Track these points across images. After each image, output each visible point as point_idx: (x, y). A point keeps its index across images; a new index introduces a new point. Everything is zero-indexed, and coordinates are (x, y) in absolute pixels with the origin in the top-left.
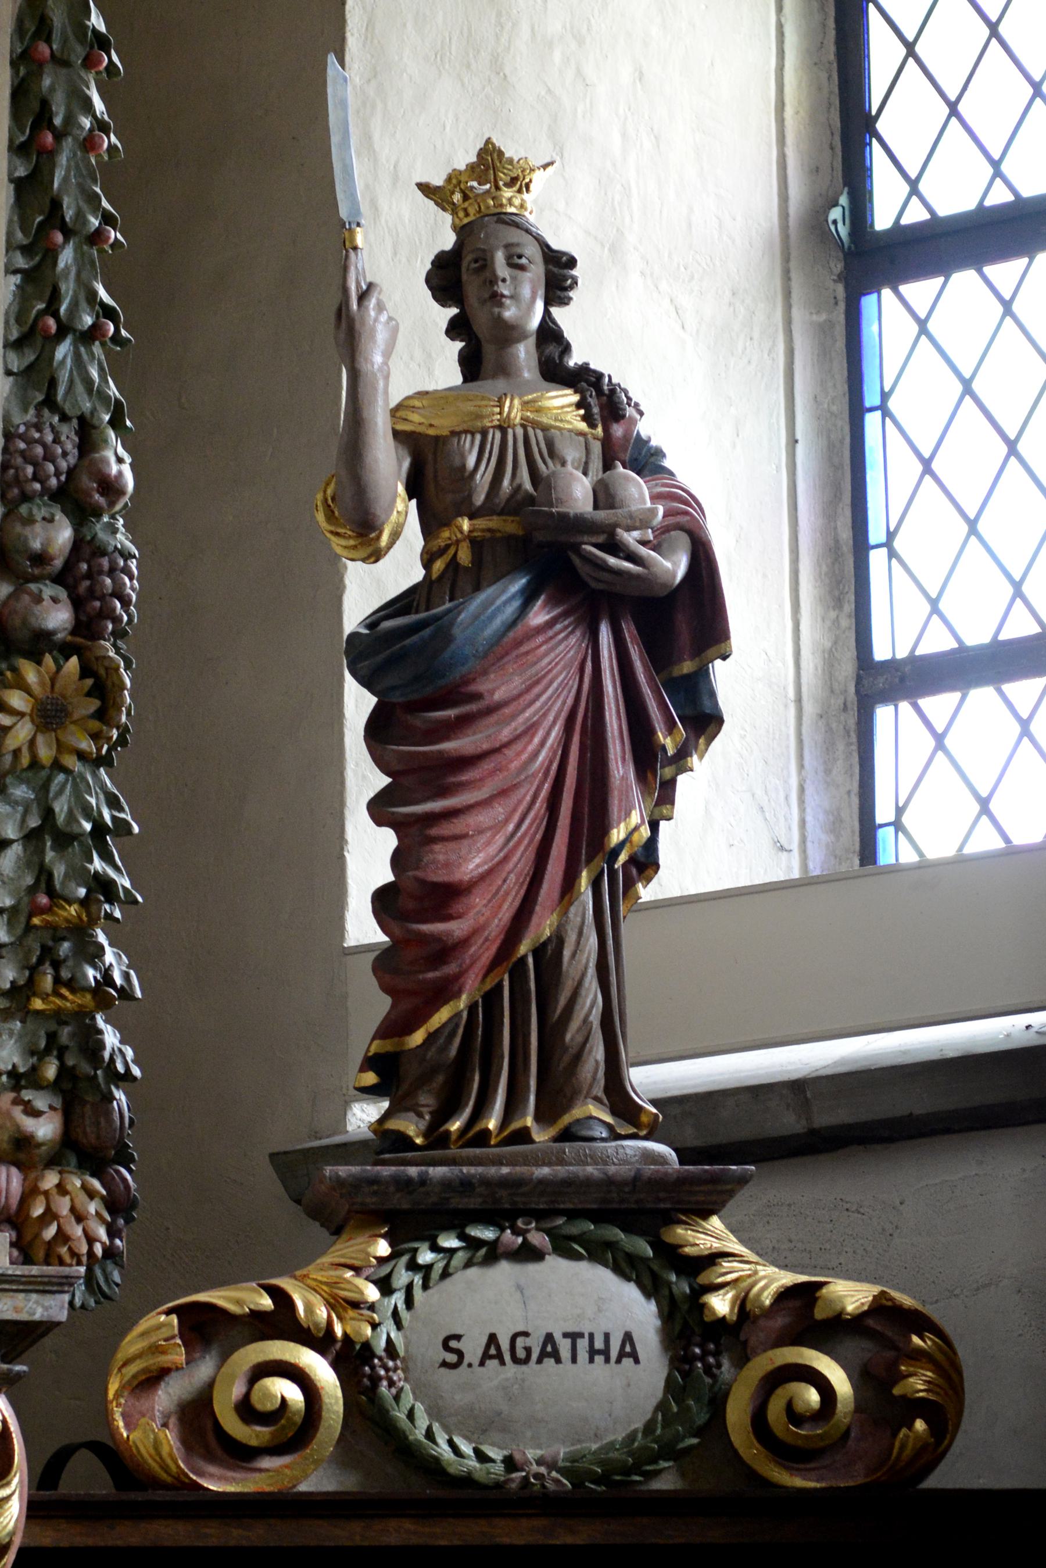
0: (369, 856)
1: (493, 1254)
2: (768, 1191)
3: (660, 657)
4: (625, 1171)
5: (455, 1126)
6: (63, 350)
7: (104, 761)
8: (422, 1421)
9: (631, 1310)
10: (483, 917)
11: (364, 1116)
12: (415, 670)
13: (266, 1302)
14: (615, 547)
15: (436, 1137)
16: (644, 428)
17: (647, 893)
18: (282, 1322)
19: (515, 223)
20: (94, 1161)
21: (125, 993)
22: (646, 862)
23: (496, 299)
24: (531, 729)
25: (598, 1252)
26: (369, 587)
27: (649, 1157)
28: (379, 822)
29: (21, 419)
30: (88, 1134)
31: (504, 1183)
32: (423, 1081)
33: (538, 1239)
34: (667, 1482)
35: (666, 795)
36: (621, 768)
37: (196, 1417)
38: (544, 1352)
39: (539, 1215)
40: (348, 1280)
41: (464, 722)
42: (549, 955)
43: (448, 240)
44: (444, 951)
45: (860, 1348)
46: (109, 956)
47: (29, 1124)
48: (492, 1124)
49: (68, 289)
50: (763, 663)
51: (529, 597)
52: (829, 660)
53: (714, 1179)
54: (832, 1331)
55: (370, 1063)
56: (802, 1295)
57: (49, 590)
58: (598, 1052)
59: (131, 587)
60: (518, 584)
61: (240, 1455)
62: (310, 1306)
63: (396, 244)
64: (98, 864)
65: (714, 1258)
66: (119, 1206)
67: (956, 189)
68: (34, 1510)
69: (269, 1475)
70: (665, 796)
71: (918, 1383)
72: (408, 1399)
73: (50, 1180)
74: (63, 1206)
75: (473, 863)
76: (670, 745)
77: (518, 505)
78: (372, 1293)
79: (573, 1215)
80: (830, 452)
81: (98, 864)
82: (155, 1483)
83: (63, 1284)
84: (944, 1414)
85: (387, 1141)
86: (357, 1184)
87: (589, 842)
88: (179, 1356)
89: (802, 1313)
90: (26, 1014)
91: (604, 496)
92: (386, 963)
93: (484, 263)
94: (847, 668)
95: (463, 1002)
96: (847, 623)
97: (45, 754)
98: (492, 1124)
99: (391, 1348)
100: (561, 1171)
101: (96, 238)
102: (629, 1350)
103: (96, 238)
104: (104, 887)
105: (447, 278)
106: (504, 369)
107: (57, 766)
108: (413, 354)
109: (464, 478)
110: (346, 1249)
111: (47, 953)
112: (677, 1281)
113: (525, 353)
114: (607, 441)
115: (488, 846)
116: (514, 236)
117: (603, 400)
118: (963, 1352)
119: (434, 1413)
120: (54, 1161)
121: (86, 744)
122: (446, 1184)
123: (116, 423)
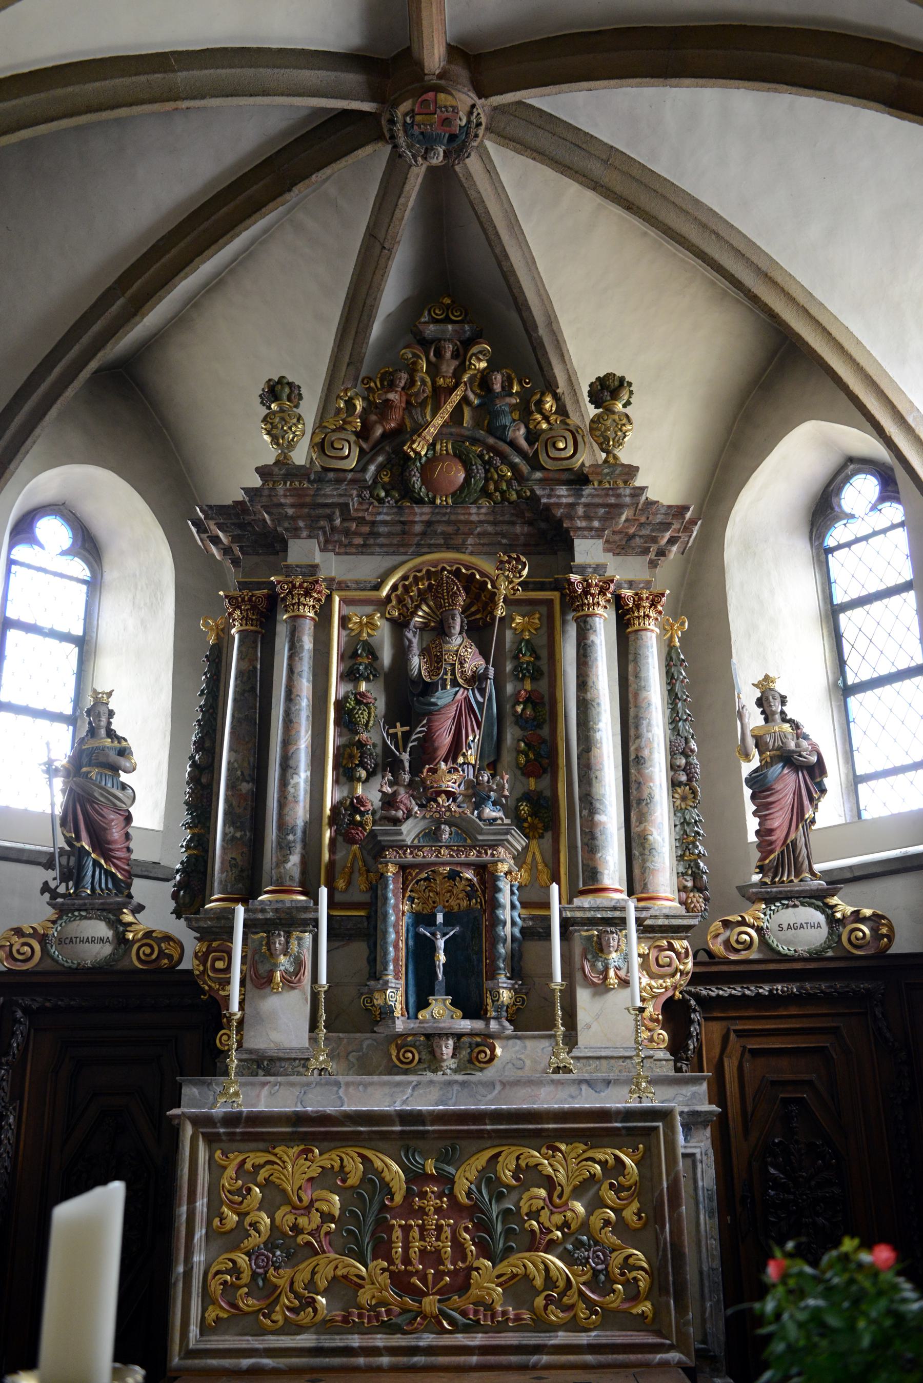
0: (753, 824)
1: (788, 906)
2: (846, 889)
3: (812, 777)
4: (815, 888)
5: (777, 880)
6: (680, 724)
7: (695, 807)
8: (775, 943)
9: (819, 917)
10: (779, 836)
11: (756, 878)
12: (760, 785)
13: (740, 919)
14: (801, 756)
15: (773, 883)
16: (804, 730)
17: (813, 828)
18: (743, 923)
19: (773, 690)
20: (700, 890)
21: (704, 855)
22: (813, 821)
23: (770, 706)
24: (786, 795)
25: (810, 905)
26: (747, 769)
27: (820, 884)
28: (755, 816)
29: (673, 738)
30: (699, 885)
31: (788, 891)
32: (769, 870)
33: (797, 903)
34: (830, 954)
35: (816, 807)
36: (806, 802)
37: (727, 943)
38: (800, 929)
39: (797, 898)
40: (756, 913)
41: (772, 794)
42: (794, 843)
43: (759, 695)
44: (771, 843)
45: (870, 923)
46: (700, 847)
47: (686, 883)
48: (785, 879)
49: (680, 711)
50: (834, 779)
51: (783, 767)
52: (847, 776)
53: (835, 888)
54: (864, 920)
55: (758, 867)
56: (857, 912)
57: (681, 773)
58: (806, 862)
59: (698, 771)
60: (781, 764)
61: (737, 951)
62: (749, 919)
63: (747, 696)
64: (696, 829)
65: (836, 905)
66: (706, 899)
67: (866, 675)
68: (695, 964)
69: (743, 955)
70: (816, 807)
71: (884, 930)
72: (772, 938)
73: (692, 895)
74: (695, 900)
75: (776, 824)
76: (816, 796)
77: (779, 748)
78: (762, 916)
79: (804, 897)
80: (843, 733)
81: (696, 829)
82: (719, 958)
83: (696, 917)
84: (890, 937)
85: (763, 884)
86: (757, 893)
87: (799, 815)
88: (722, 931)
89: (857, 916)
90: (683, 860)
91: (797, 745)
92: (759, 846)
93: (767, 699)
94: (851, 777)
95: (776, 853)
96: (850, 767)
97: (683, 806)
98: (785, 879)
99: (767, 928)
100: (801, 888)
101: (685, 700)
102: (819, 926)
103: (685, 700)
104: (698, 833)
105: (760, 702)
106: (773, 720)
107: (686, 809)
108: (754, 719)
109: (767, 744)
110: (756, 906)
111: (687, 847)
112: (828, 911)
113: (778, 717)
114: (797, 734)
115: (779, 820)
116: (773, 693)
117: (796, 726)
118: (894, 925)
119: (778, 941)
120: (692, 891)
121: (692, 804)
122: (776, 892)
123: (692, 737)
